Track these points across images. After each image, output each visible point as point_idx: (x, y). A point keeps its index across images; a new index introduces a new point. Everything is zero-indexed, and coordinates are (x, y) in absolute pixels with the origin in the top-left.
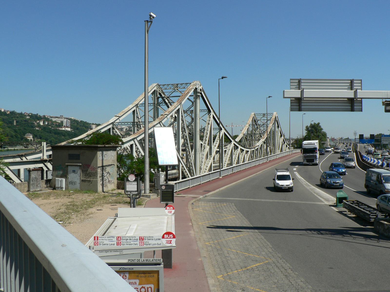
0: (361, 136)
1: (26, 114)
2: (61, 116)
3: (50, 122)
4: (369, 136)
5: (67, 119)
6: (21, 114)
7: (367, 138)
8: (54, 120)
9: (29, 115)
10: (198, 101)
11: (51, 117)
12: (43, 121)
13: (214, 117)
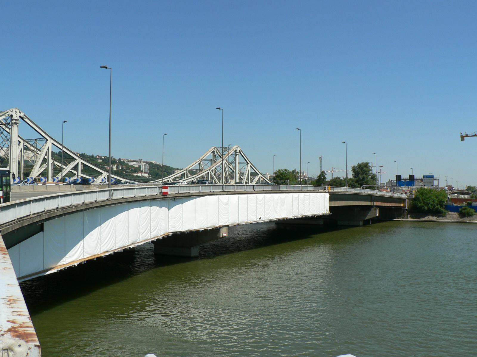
0: (399, 177)
1: (98, 157)
2: (139, 159)
3: (125, 166)
4: (407, 177)
5: (147, 163)
6: (93, 156)
7: (405, 180)
8: (130, 164)
9: (101, 158)
10: (237, 157)
11: (129, 161)
12: (117, 165)
13: (251, 166)
